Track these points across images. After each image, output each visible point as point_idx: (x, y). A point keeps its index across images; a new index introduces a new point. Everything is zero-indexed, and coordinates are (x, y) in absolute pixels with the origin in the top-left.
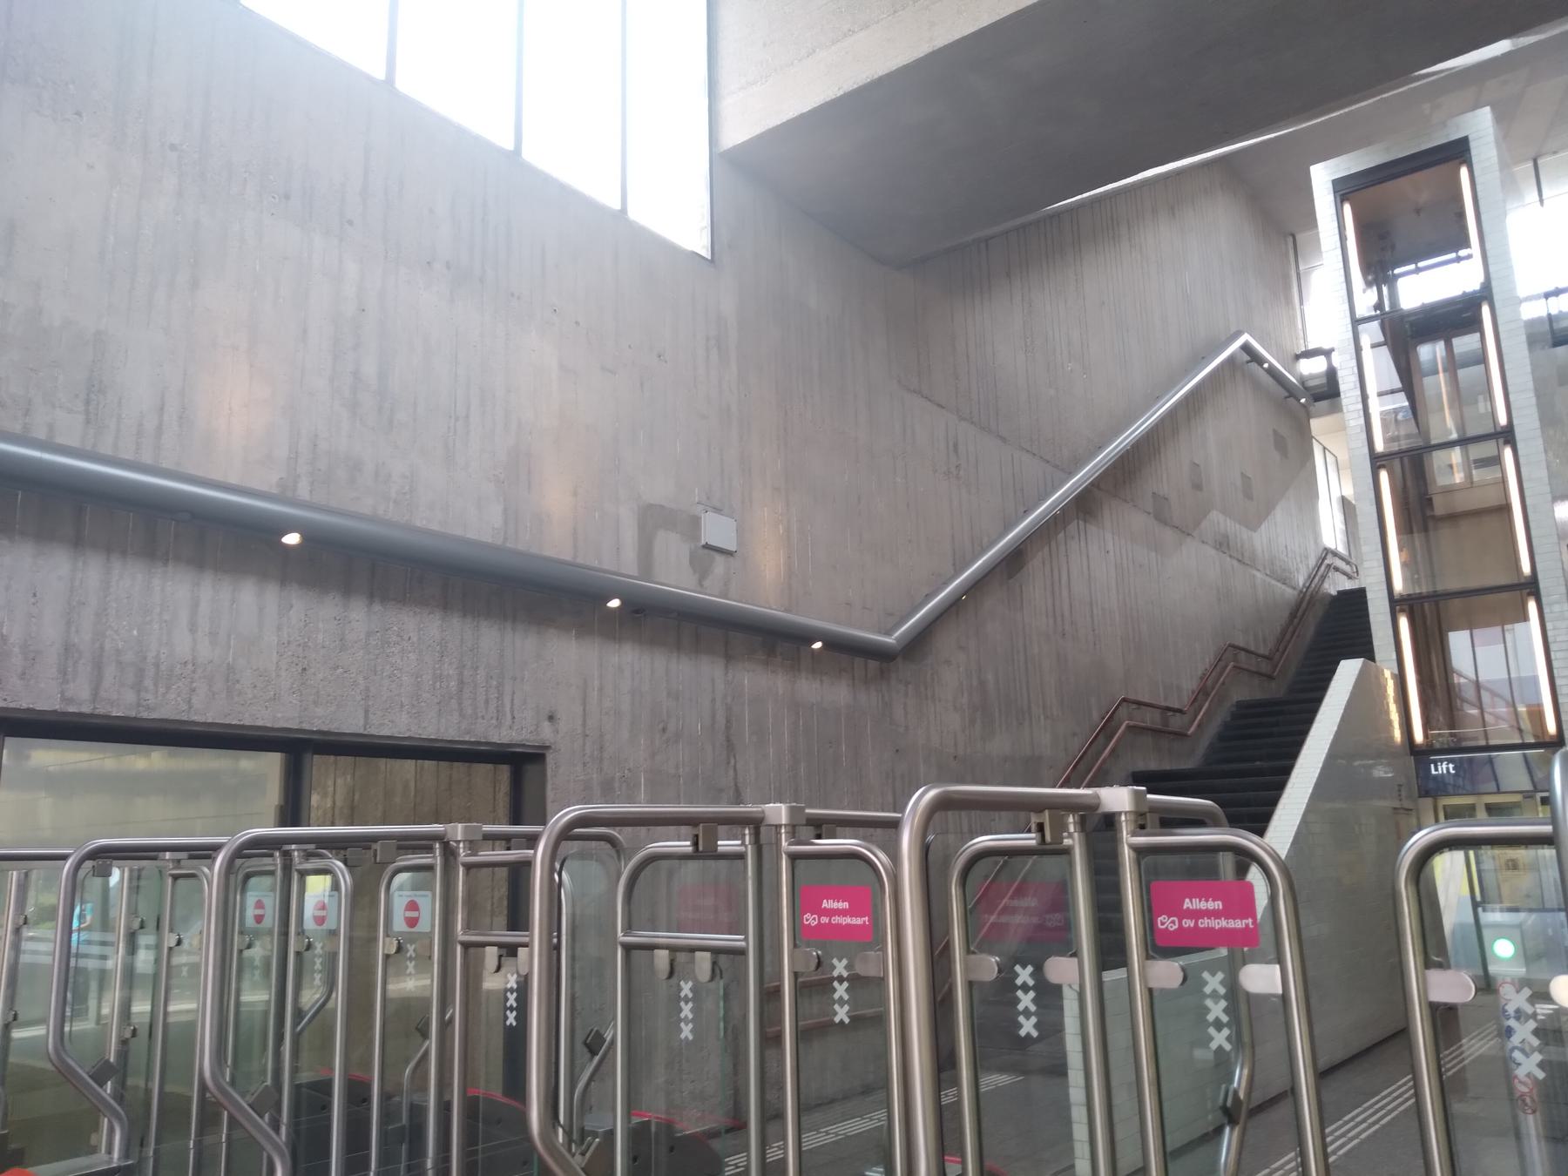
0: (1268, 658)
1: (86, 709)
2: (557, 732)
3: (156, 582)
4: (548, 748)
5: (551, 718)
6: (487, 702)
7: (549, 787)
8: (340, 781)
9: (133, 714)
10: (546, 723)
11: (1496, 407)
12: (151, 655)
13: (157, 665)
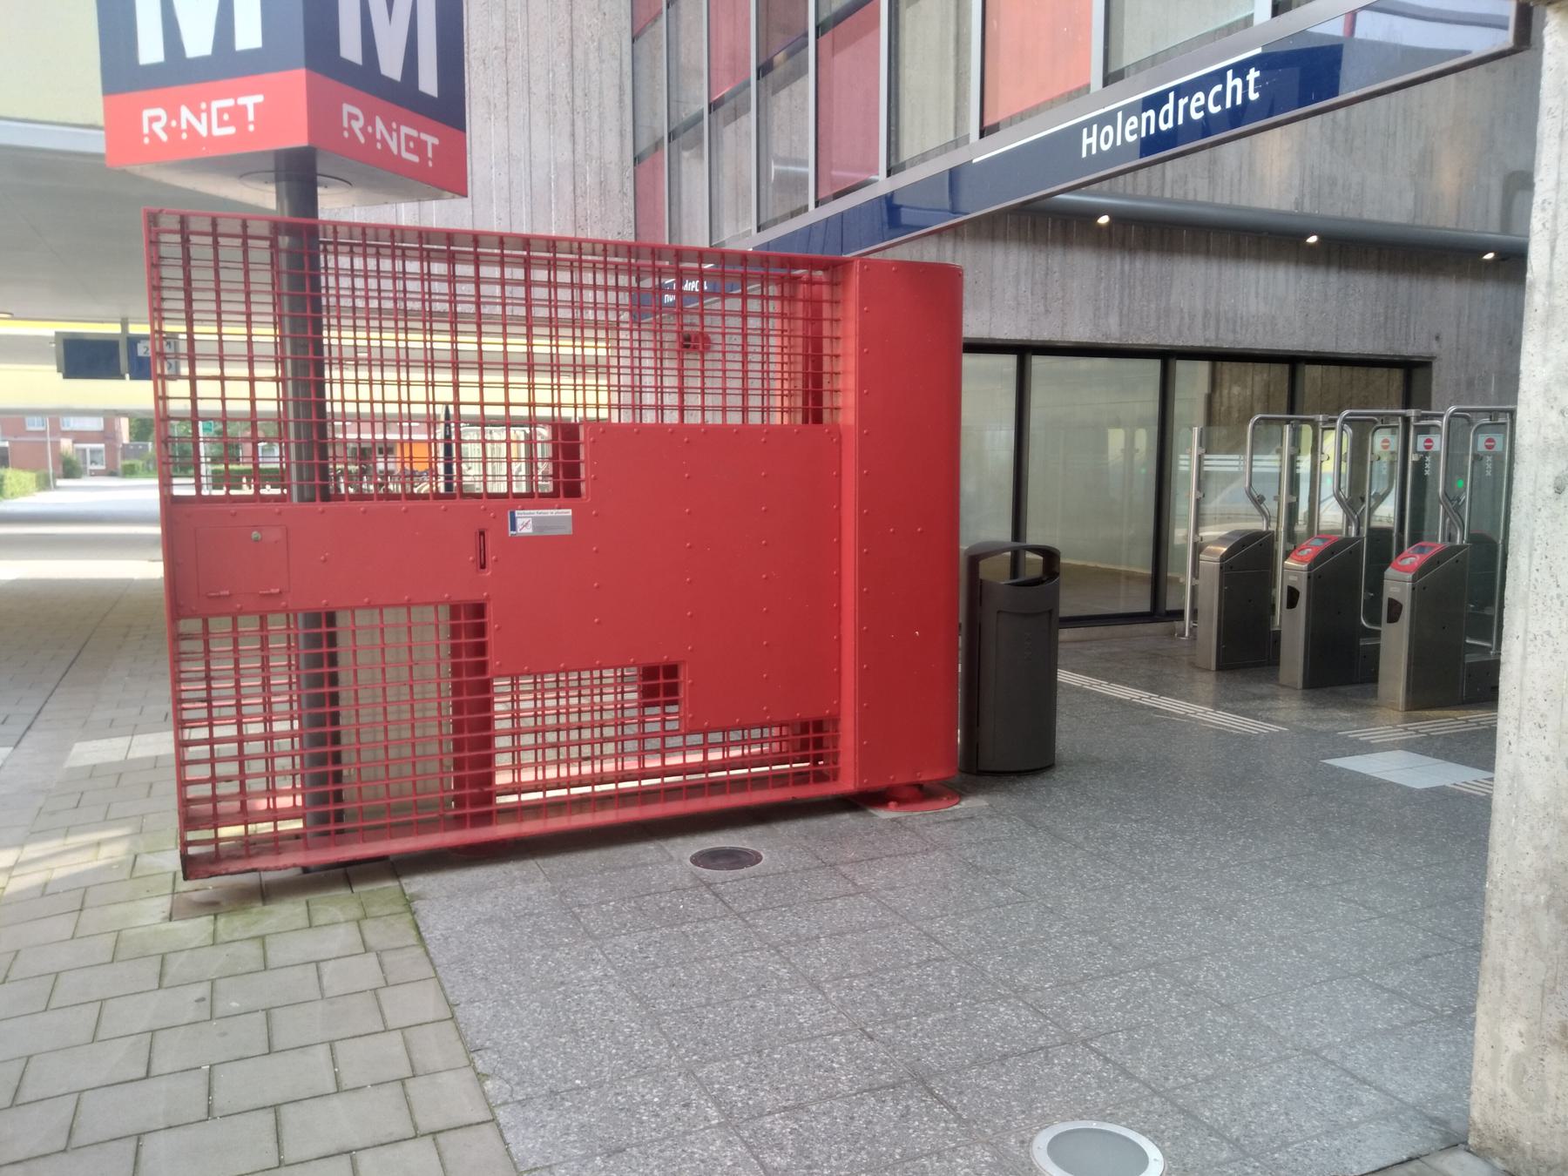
0: (164, 319)
1: (1213, 345)
2: (1440, 347)
3: (1241, 271)
4: (1433, 358)
5: (1437, 338)
6: (1400, 329)
7: (1434, 383)
8: (1257, 378)
9: (1232, 346)
10: (1434, 342)
11: (1453, 13)
12: (1239, 312)
13: (1242, 318)
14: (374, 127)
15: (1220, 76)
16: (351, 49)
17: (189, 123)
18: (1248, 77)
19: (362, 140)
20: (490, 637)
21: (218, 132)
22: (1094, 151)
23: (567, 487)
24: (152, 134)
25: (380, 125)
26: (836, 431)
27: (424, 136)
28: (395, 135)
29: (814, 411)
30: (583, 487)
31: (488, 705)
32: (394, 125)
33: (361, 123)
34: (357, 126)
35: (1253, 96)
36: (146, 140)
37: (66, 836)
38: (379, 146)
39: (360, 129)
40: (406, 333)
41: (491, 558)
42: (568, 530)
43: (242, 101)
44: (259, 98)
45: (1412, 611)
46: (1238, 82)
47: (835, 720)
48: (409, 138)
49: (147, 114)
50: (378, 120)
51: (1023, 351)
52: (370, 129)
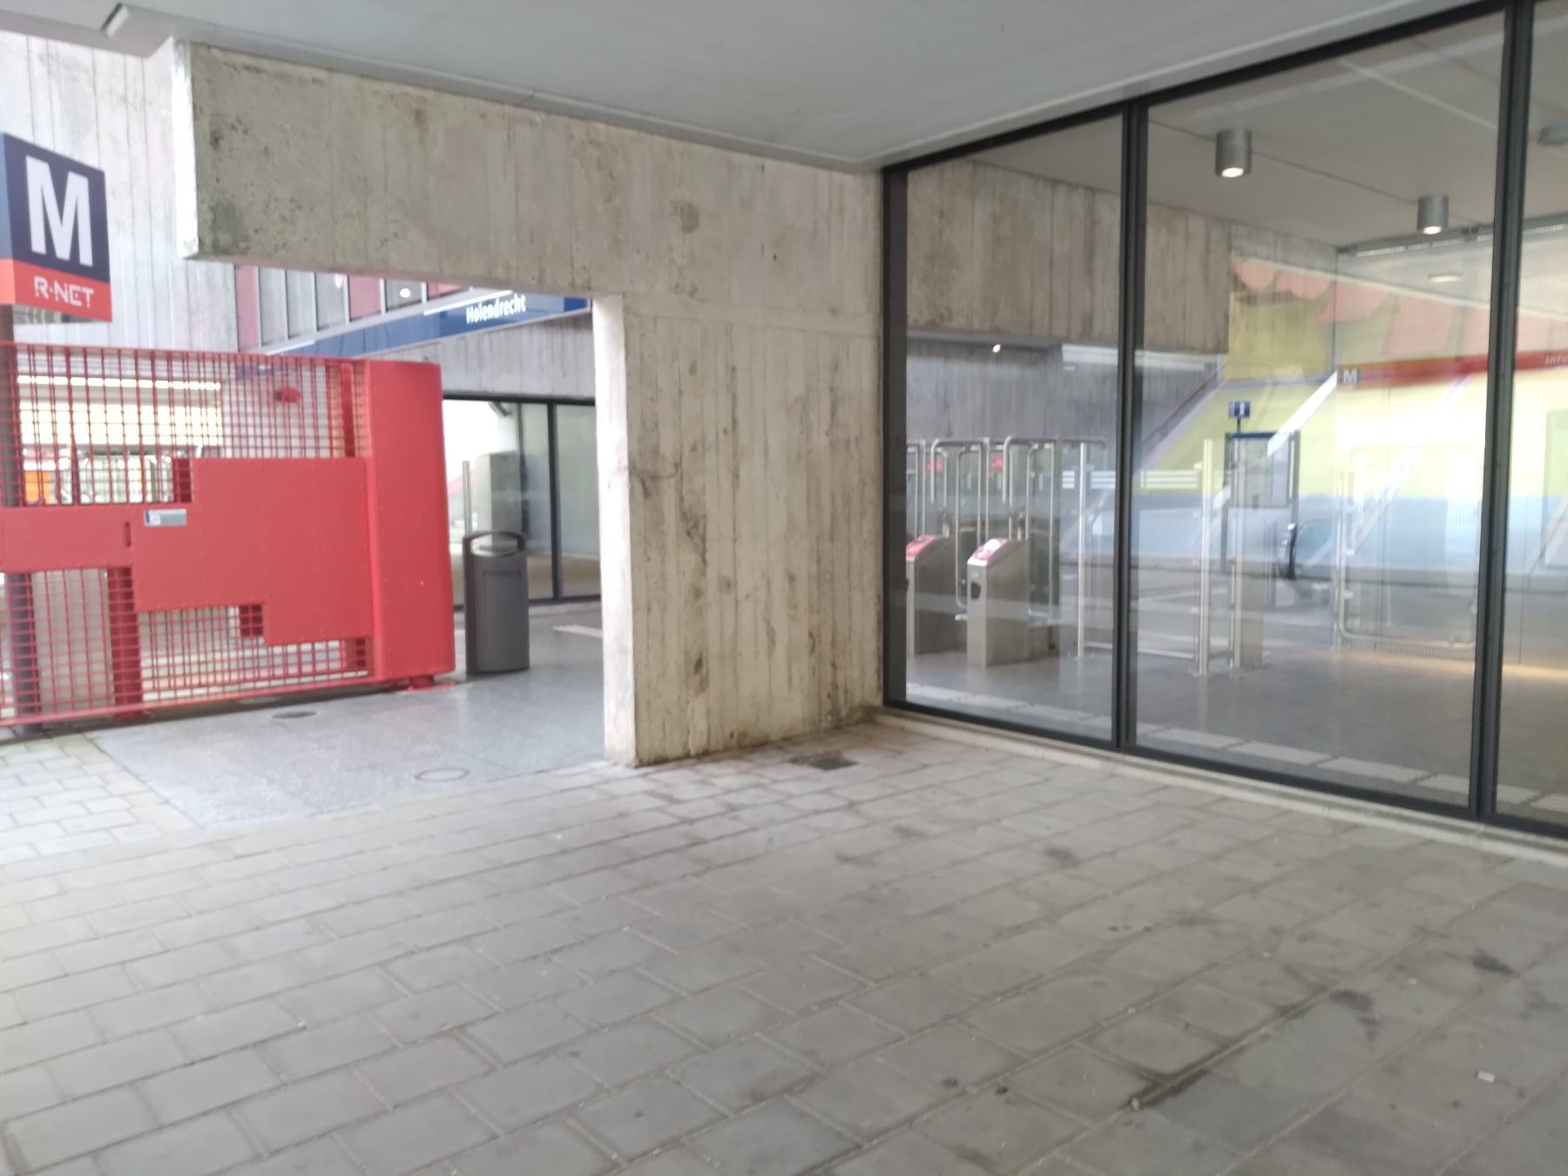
14: (54, 288)
16: (38, 245)
19: (46, 296)
20: (135, 588)
23: (182, 494)
25: (57, 286)
26: (363, 463)
28: (66, 291)
29: (350, 451)
30: (193, 497)
31: (137, 664)
32: (66, 285)
34: (44, 289)
37: (532, 97)
40: (92, 460)
41: (134, 539)
42: (184, 522)
45: (916, 582)
47: (371, 637)
48: (74, 292)
51: (551, 403)
52: (51, 290)
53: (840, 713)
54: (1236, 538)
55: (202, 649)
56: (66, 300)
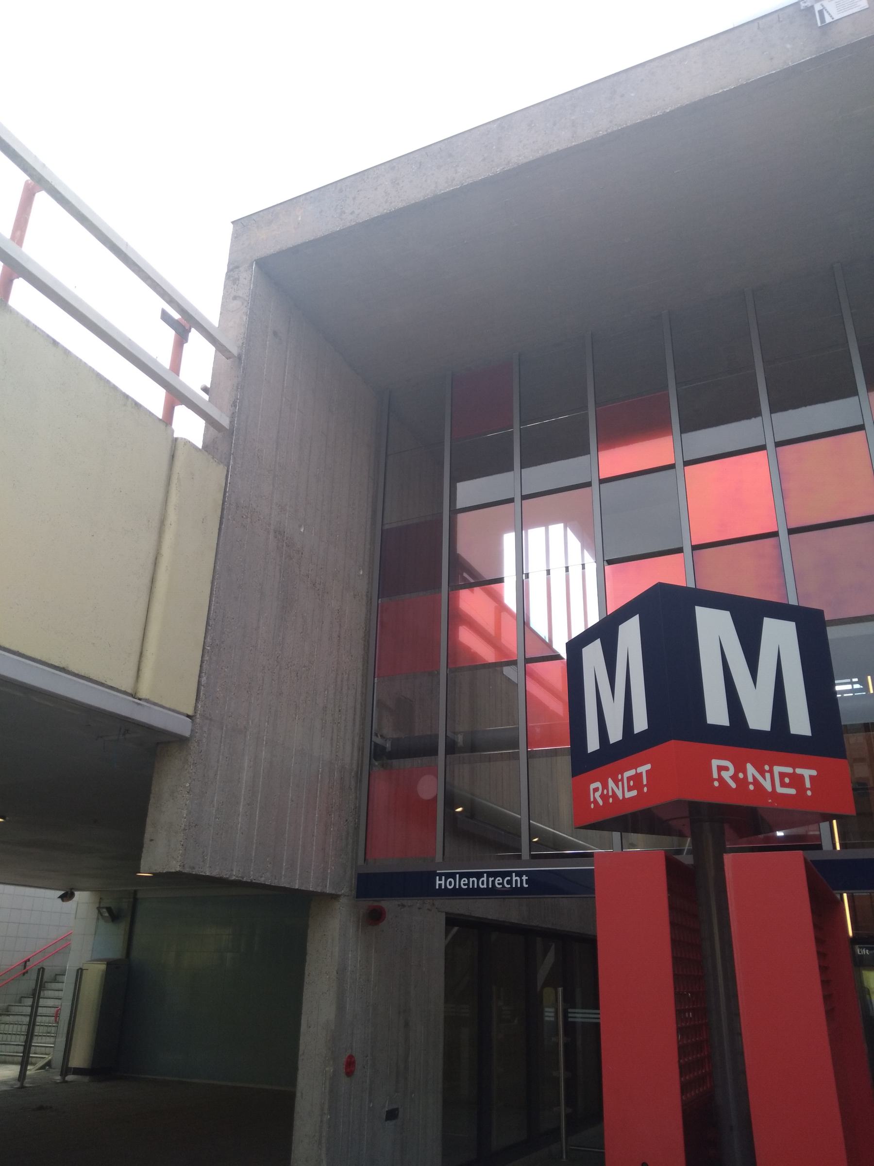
15: (509, 874)
17: (754, 777)
18: (523, 878)
19: (733, 785)
21: (780, 790)
22: (443, 887)
24: (721, 779)
25: (751, 770)
27: (799, 771)
28: (768, 775)
32: (767, 768)
33: (732, 771)
34: (726, 775)
35: (525, 886)
36: (592, 806)
38: (751, 787)
39: (732, 777)
43: (640, 770)
44: (648, 767)
46: (518, 878)
48: (782, 775)
49: (593, 786)
50: (749, 766)
52: (741, 775)
53: (384, 748)
54: (575, 1013)
55: (838, 6)
56: (769, 789)
